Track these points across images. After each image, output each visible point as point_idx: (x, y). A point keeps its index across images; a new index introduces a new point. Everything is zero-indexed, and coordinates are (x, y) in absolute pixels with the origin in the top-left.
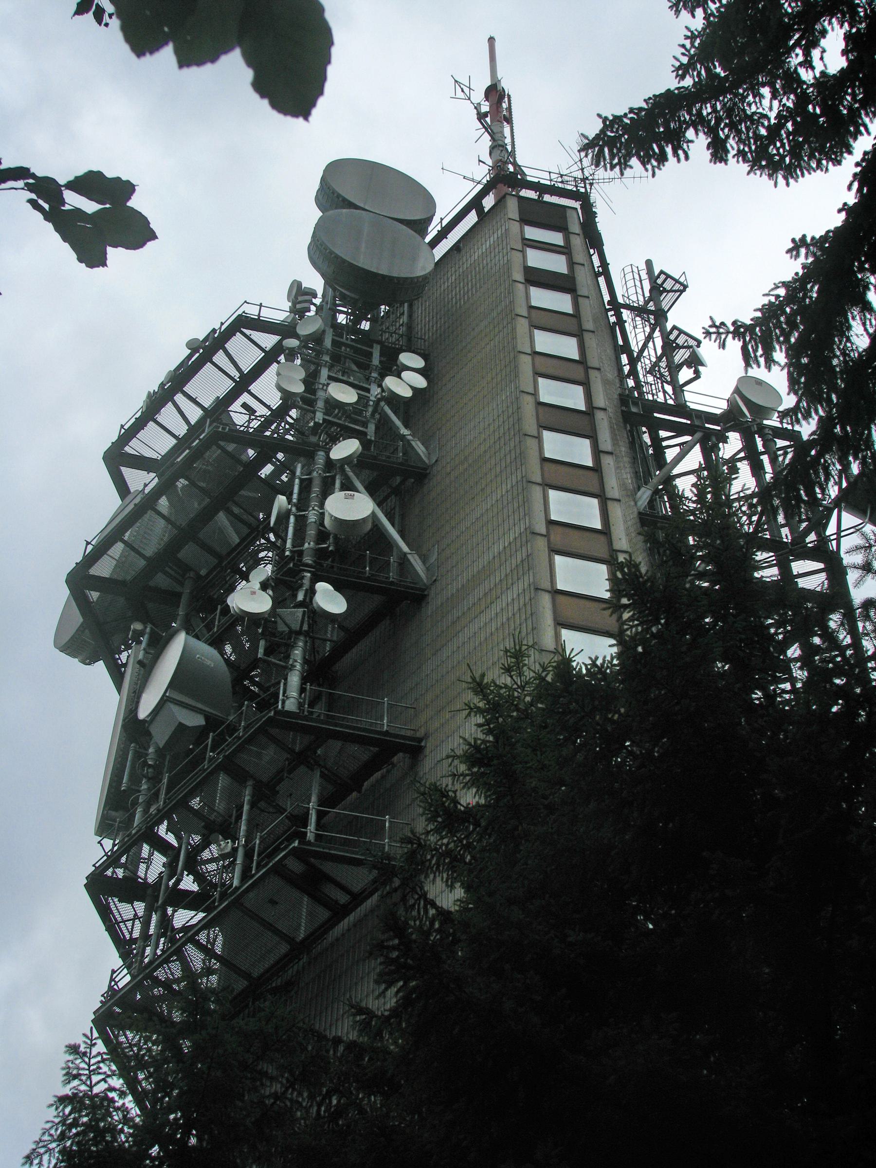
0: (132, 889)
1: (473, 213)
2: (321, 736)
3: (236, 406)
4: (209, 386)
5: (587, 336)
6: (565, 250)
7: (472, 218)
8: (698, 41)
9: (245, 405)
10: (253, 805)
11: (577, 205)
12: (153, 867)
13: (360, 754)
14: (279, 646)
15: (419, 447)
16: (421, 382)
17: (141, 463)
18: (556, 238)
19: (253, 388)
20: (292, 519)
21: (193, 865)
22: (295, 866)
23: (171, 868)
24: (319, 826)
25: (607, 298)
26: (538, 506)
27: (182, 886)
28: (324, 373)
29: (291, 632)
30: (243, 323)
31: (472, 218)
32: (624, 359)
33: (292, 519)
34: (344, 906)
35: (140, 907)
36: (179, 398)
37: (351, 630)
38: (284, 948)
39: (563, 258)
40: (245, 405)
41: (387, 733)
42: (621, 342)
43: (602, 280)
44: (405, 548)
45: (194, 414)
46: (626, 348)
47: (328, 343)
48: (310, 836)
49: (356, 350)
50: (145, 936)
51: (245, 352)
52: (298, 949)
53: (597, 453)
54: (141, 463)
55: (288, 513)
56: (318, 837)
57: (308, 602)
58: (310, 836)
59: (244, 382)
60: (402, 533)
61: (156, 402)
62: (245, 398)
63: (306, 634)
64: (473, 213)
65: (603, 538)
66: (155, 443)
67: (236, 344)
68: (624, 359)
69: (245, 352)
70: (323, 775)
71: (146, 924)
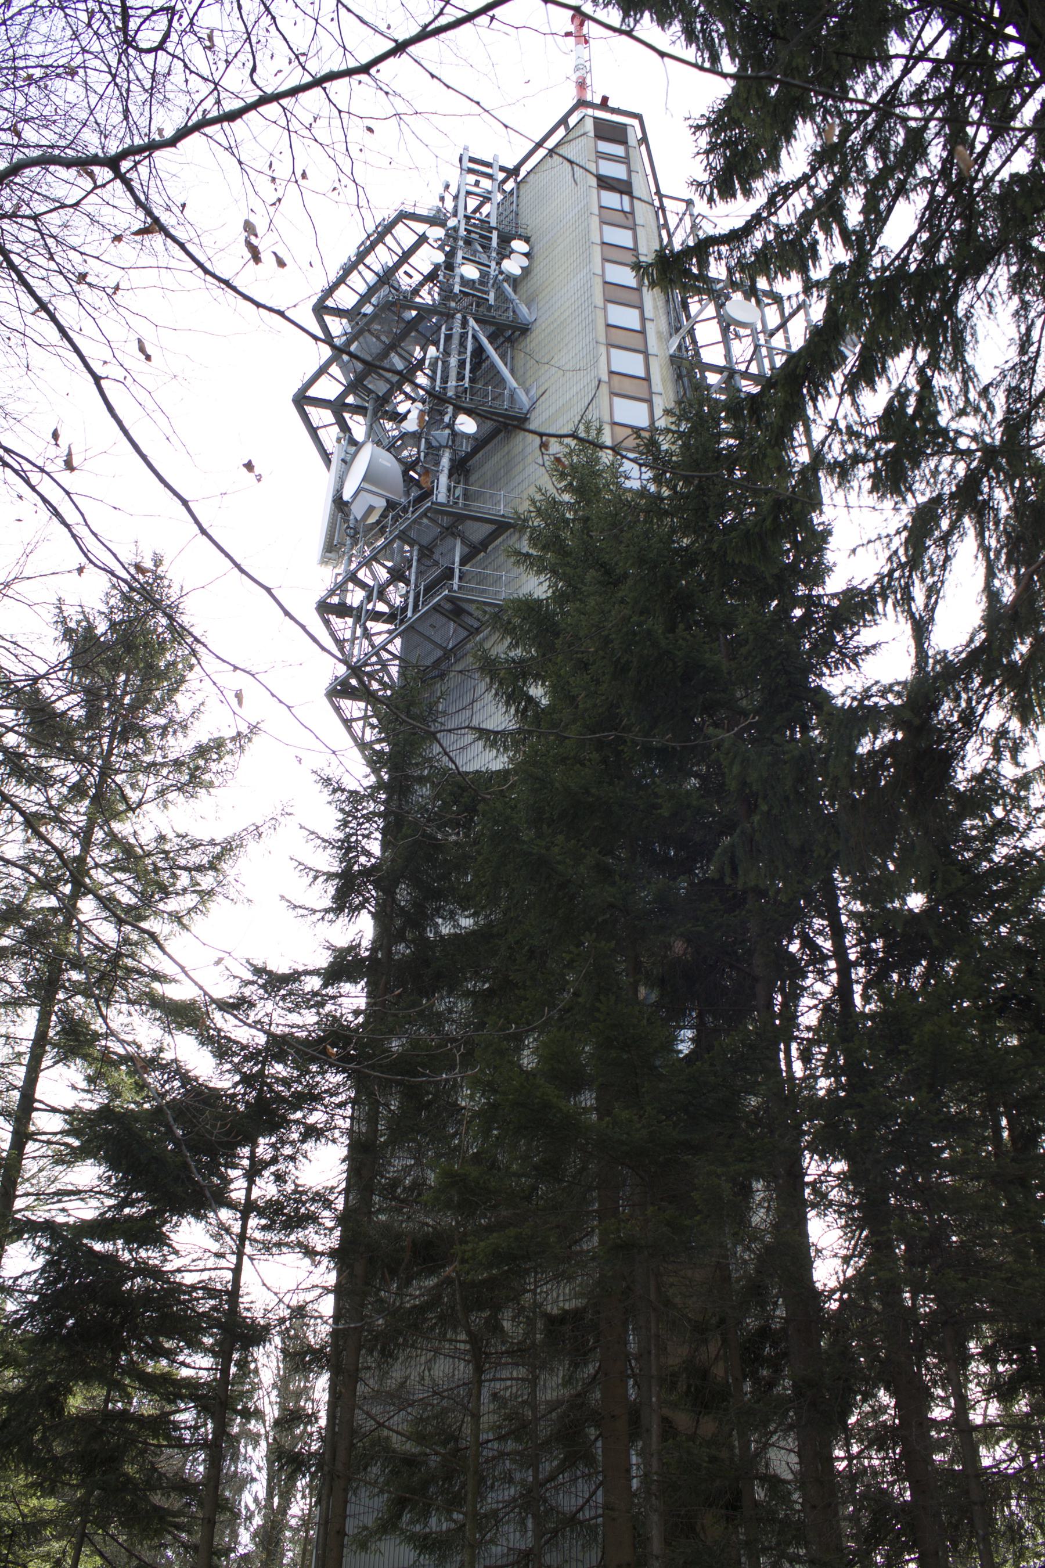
0: (342, 610)
1: (562, 128)
2: (461, 518)
3: (401, 271)
4: (382, 257)
5: (639, 230)
6: (626, 160)
7: (561, 132)
8: (952, 1400)
9: (406, 273)
10: (418, 560)
11: (635, 122)
12: (355, 597)
13: (489, 528)
14: (434, 451)
15: (524, 309)
16: (525, 262)
17: (338, 312)
18: (618, 150)
19: (411, 261)
20: (440, 363)
21: (382, 596)
22: (448, 606)
23: (369, 598)
24: (460, 578)
25: (653, 190)
26: (603, 359)
27: (377, 609)
28: (460, 254)
29: (441, 446)
30: (403, 216)
31: (561, 132)
32: (664, 233)
33: (440, 363)
34: (477, 629)
35: (350, 621)
36: (361, 267)
37: (480, 442)
38: (439, 653)
39: (623, 167)
40: (406, 273)
41: (503, 516)
42: (662, 222)
43: (643, 148)
44: (515, 385)
45: (371, 278)
46: (666, 225)
47: (462, 232)
48: (455, 587)
49: (481, 236)
50: (354, 638)
51: (405, 235)
52: (447, 654)
53: (643, 319)
54: (338, 312)
55: (437, 358)
56: (460, 587)
57: (451, 426)
58: (455, 587)
59: (406, 256)
60: (512, 372)
61: (349, 269)
62: (406, 267)
63: (451, 447)
64: (562, 128)
65: (645, 383)
66: (345, 298)
67: (400, 230)
68: (664, 233)
69: (405, 235)
70: (463, 542)
71: (354, 632)
